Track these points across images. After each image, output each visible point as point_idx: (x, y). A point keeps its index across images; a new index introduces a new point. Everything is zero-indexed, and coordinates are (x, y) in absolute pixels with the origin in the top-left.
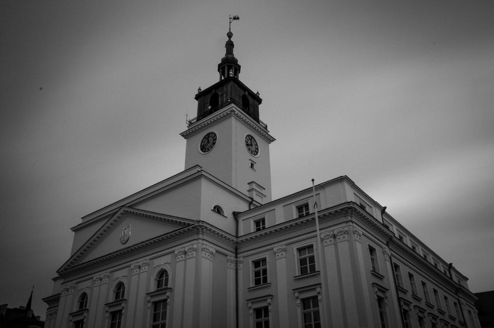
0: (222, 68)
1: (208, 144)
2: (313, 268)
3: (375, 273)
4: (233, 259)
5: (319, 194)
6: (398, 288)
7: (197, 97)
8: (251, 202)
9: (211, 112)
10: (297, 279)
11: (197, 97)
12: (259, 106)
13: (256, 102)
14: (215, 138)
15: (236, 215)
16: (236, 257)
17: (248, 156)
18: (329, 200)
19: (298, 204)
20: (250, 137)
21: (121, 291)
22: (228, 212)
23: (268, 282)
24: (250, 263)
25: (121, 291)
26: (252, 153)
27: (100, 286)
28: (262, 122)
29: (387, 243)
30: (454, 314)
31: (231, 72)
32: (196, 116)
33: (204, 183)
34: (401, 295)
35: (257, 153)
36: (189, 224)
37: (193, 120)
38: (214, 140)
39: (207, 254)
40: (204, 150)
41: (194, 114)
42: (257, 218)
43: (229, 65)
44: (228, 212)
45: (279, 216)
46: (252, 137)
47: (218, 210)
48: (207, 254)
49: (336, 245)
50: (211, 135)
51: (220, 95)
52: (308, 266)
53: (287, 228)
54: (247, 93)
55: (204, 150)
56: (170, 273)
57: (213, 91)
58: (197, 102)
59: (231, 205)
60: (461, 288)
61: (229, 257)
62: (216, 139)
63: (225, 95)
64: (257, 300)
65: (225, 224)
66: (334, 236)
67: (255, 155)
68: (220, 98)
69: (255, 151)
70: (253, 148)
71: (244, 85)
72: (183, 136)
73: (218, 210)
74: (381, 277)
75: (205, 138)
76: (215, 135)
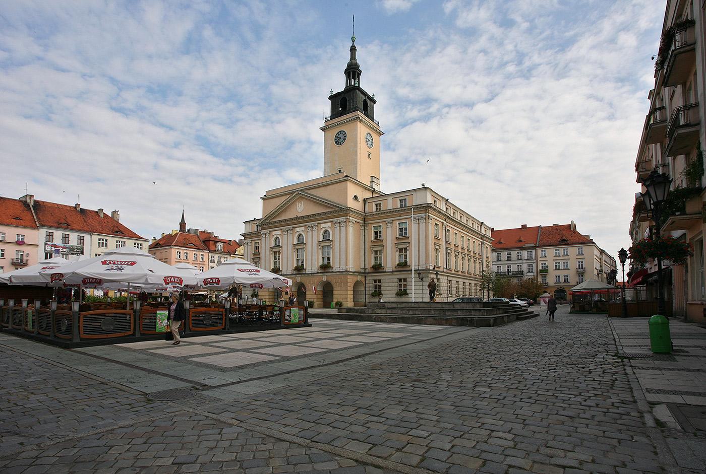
0: (347, 72)
1: (340, 140)
2: (406, 234)
3: (436, 238)
7: (330, 98)
8: (373, 191)
9: (341, 114)
10: (397, 239)
11: (330, 98)
12: (374, 105)
13: (372, 103)
14: (345, 135)
15: (365, 201)
18: (417, 200)
19: (400, 198)
22: (360, 199)
30: (477, 251)
33: (348, 183)
41: (328, 112)
43: (353, 71)
44: (360, 199)
45: (389, 205)
47: (356, 197)
50: (342, 132)
52: (403, 234)
53: (392, 213)
54: (366, 97)
56: (331, 232)
57: (343, 95)
59: (364, 195)
60: (667, 75)
65: (357, 206)
68: (347, 102)
70: (370, 143)
72: (322, 129)
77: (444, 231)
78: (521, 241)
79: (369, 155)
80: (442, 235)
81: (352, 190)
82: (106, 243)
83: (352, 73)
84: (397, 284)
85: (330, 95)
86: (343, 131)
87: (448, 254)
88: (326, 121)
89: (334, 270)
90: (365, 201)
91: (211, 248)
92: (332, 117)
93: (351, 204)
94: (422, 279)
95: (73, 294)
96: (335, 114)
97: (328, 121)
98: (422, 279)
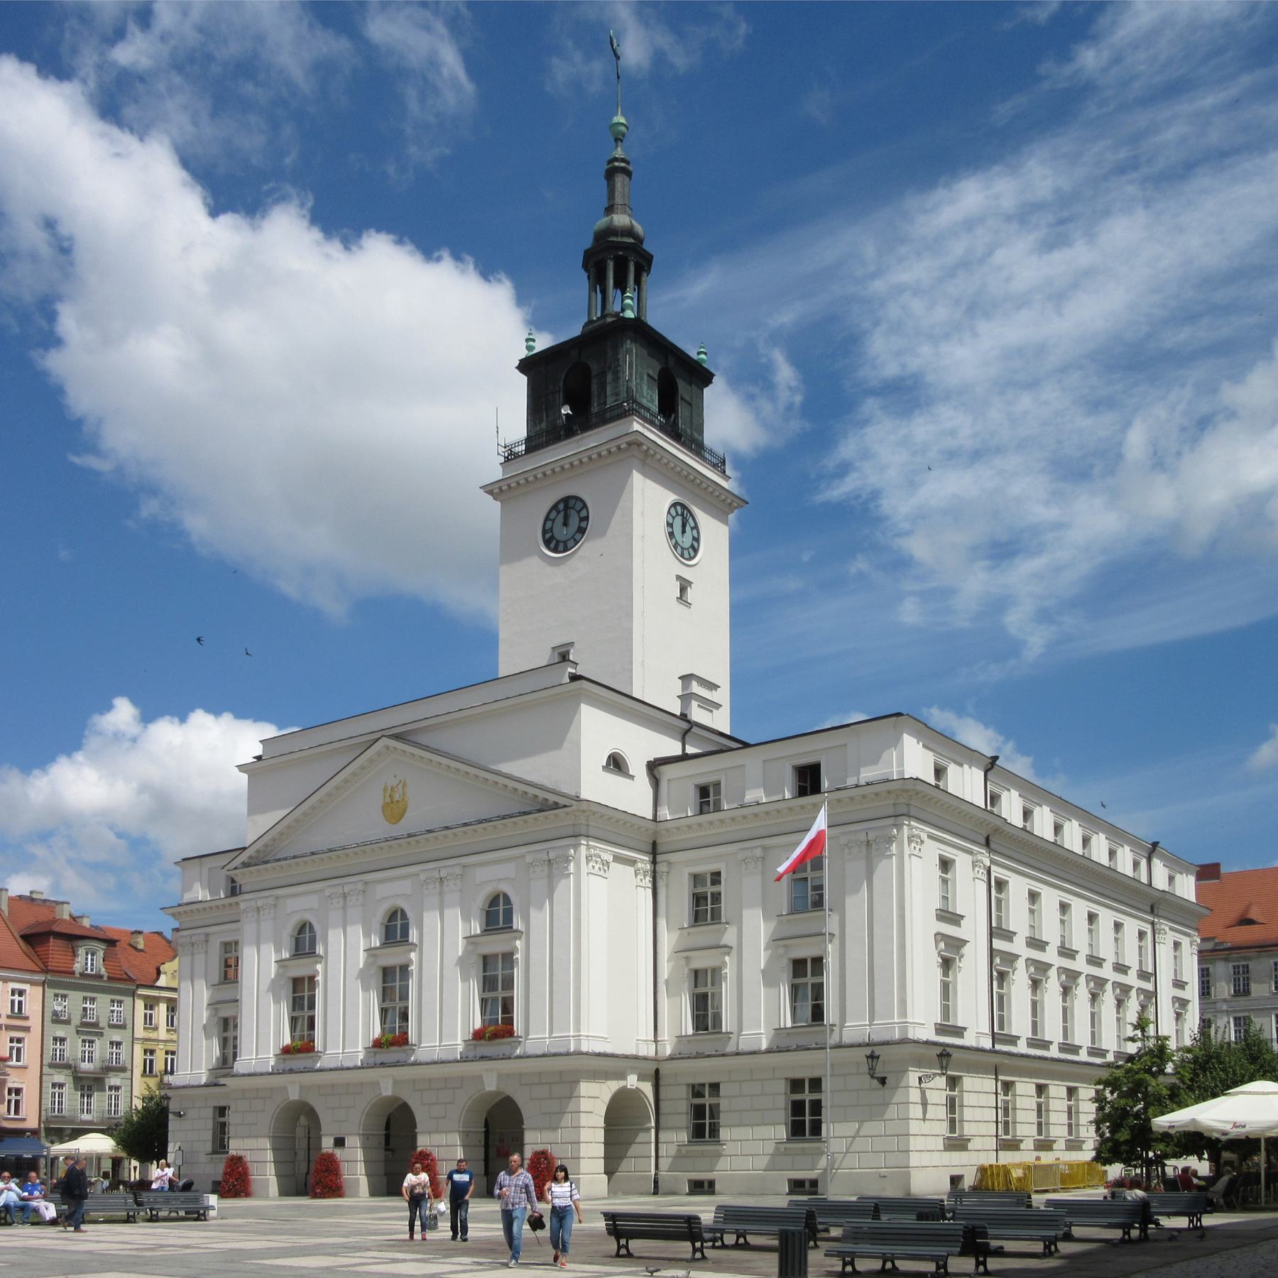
4: (648, 867)
5: (845, 745)
6: (997, 931)
9: (569, 430)
11: (524, 366)
14: (583, 513)
15: (654, 767)
16: (654, 862)
17: (672, 566)
20: (679, 508)
21: (399, 923)
22: (638, 767)
23: (723, 920)
24: (686, 876)
25: (399, 923)
26: (682, 556)
27: (854, 1137)
28: (711, 452)
29: (987, 839)
31: (628, 301)
32: (524, 434)
34: (998, 944)
35: (696, 551)
36: (556, 803)
37: (518, 444)
38: (581, 520)
39: (597, 867)
40: (552, 545)
41: (516, 427)
42: (703, 781)
44: (638, 767)
46: (684, 507)
47: (616, 764)
48: (597, 867)
49: (258, 921)
50: (571, 503)
51: (594, 373)
55: (552, 545)
58: (523, 380)
61: (639, 865)
62: (587, 518)
63: (609, 377)
64: (453, 764)
65: (634, 796)
66: (193, 944)
67: (691, 558)
69: (692, 546)
70: (687, 541)
71: (664, 338)
72: (491, 493)
73: (616, 764)
74: (955, 919)
75: (555, 507)
76: (585, 506)
77: (983, 887)
78: (1250, 922)
79: (683, 590)
80: (971, 896)
81: (599, 731)
82: (17, 1102)
83: (611, 265)
84: (210, 1124)
85: (524, 353)
86: (582, 501)
87: (1000, 977)
88: (507, 459)
89: (420, 1055)
90: (654, 767)
91: (52, 964)
92: (535, 442)
93: (597, 787)
94: (883, 1081)
95: (1182, 1222)
96: (546, 428)
97: (517, 456)
98: (883, 1081)
